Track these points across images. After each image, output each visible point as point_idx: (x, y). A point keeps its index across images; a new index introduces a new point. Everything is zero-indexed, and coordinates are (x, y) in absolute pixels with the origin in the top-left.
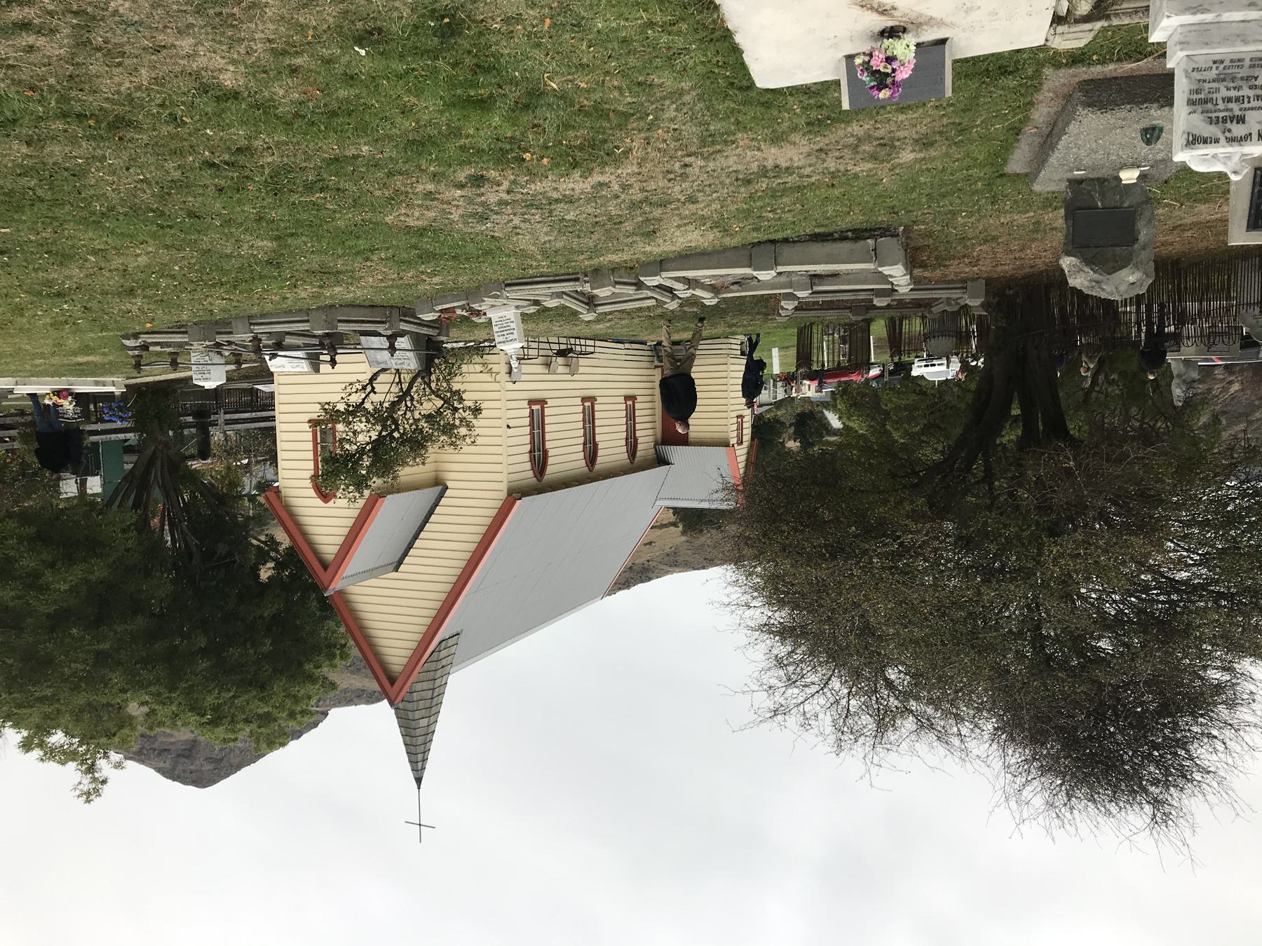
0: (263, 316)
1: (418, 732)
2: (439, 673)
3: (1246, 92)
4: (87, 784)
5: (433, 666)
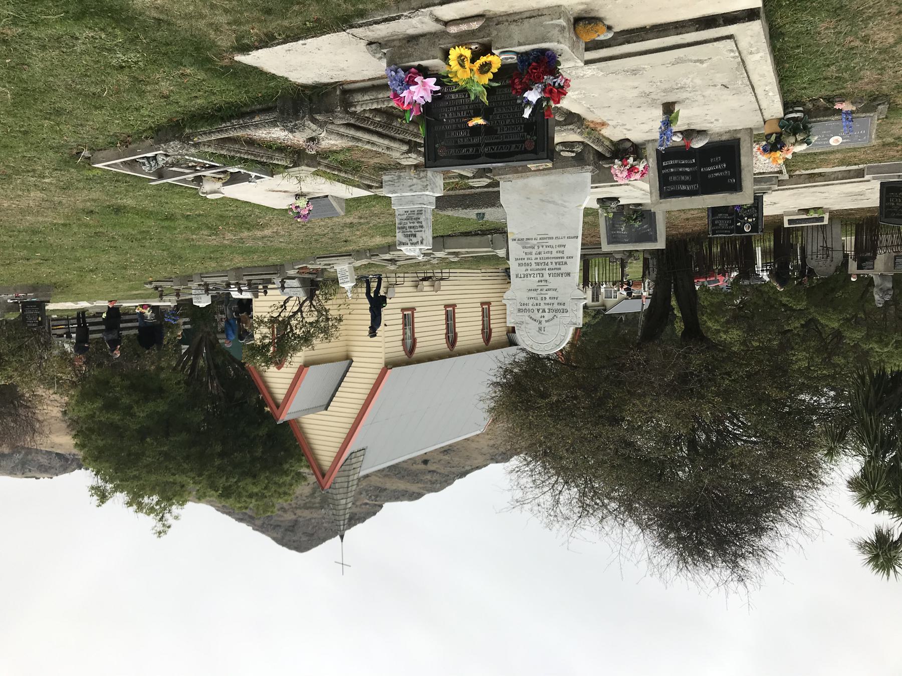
0: (207, 273)
1: (340, 507)
2: (352, 472)
3: (416, 224)
4: (160, 527)
5: (347, 468)
